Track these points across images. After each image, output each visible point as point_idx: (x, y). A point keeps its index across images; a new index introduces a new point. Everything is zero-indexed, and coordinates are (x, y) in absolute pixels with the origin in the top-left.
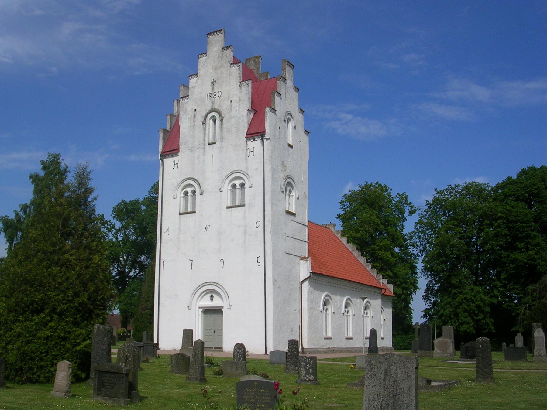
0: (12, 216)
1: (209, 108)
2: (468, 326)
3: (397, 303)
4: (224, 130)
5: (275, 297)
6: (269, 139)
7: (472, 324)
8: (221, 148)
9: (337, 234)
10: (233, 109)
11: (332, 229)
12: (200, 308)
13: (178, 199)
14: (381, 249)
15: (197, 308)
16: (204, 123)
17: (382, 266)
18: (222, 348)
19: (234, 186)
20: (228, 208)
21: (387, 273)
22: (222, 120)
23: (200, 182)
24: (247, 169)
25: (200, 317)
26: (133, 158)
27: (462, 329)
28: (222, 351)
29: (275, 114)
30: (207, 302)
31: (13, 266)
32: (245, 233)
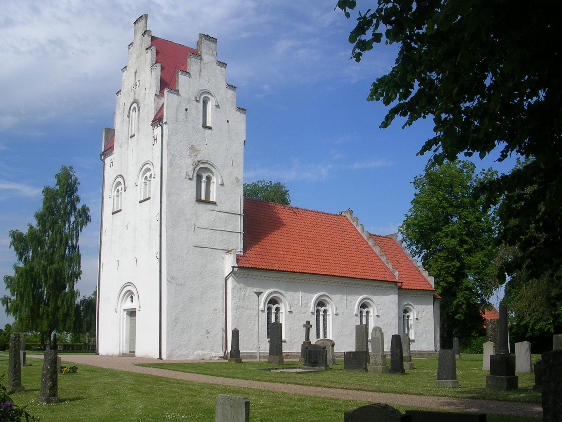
0: (25, 231)
1: (132, 100)
2: (545, 323)
3: (470, 298)
4: (140, 120)
5: (169, 294)
6: (166, 123)
7: (551, 321)
8: (138, 140)
9: (353, 221)
10: (146, 97)
11: (349, 217)
12: (125, 310)
13: (112, 198)
14: (446, 236)
15: (122, 310)
16: (128, 116)
17: (447, 256)
18: (134, 352)
19: (146, 178)
20: (141, 202)
21: (453, 263)
22: (139, 110)
23: (124, 178)
24: (153, 158)
25: (123, 319)
26: (357, 166)
27: (536, 328)
28: (134, 356)
29: (178, 94)
30: (129, 305)
31: (474, 284)
32: (150, 227)
